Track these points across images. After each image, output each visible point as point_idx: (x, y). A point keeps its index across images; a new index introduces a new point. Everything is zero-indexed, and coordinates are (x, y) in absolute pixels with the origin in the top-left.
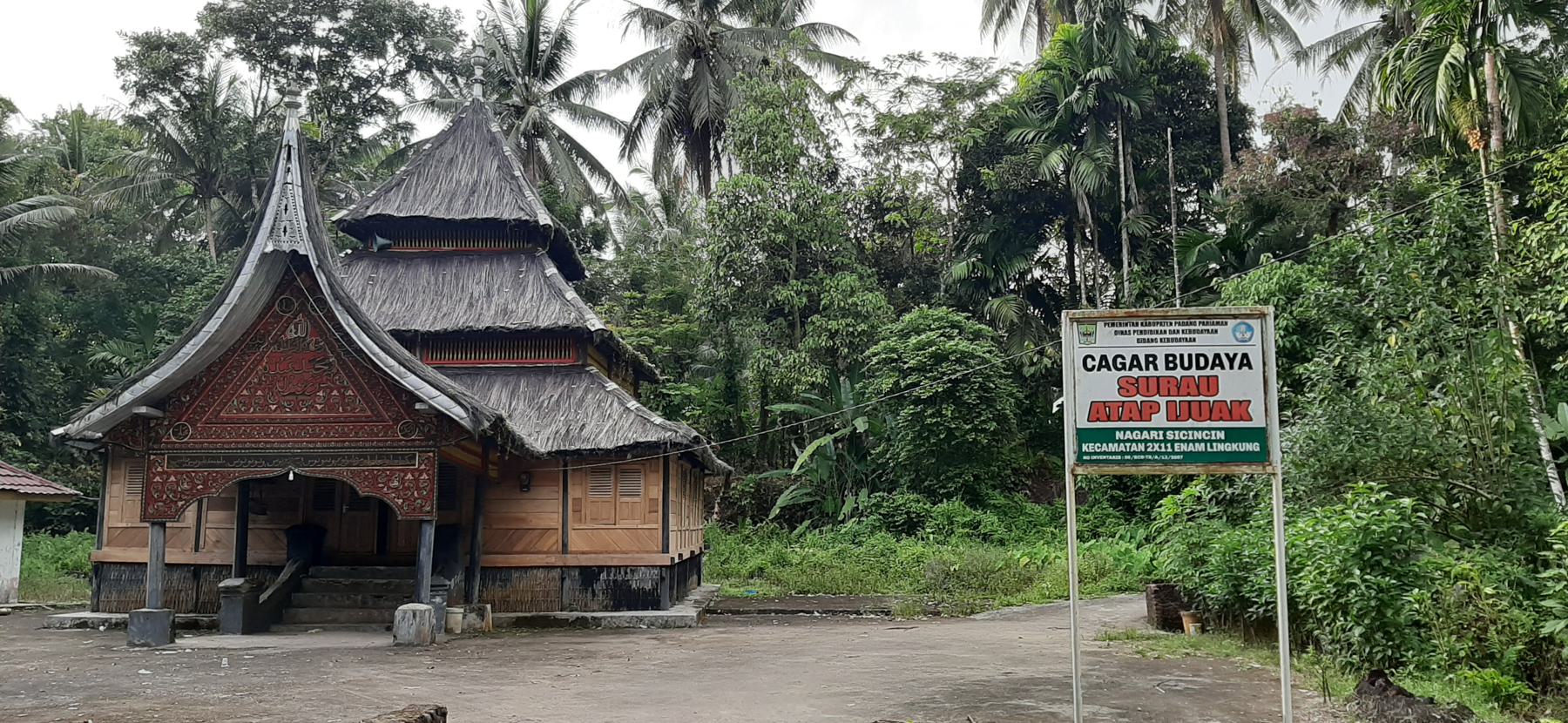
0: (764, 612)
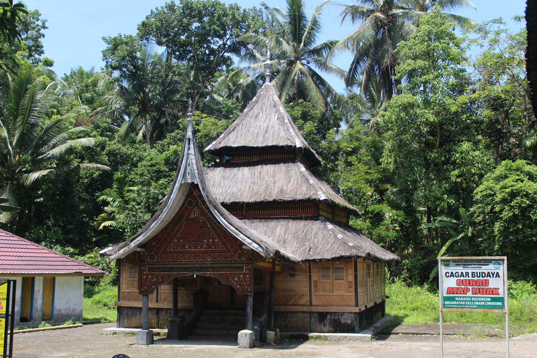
0: (406, 334)
